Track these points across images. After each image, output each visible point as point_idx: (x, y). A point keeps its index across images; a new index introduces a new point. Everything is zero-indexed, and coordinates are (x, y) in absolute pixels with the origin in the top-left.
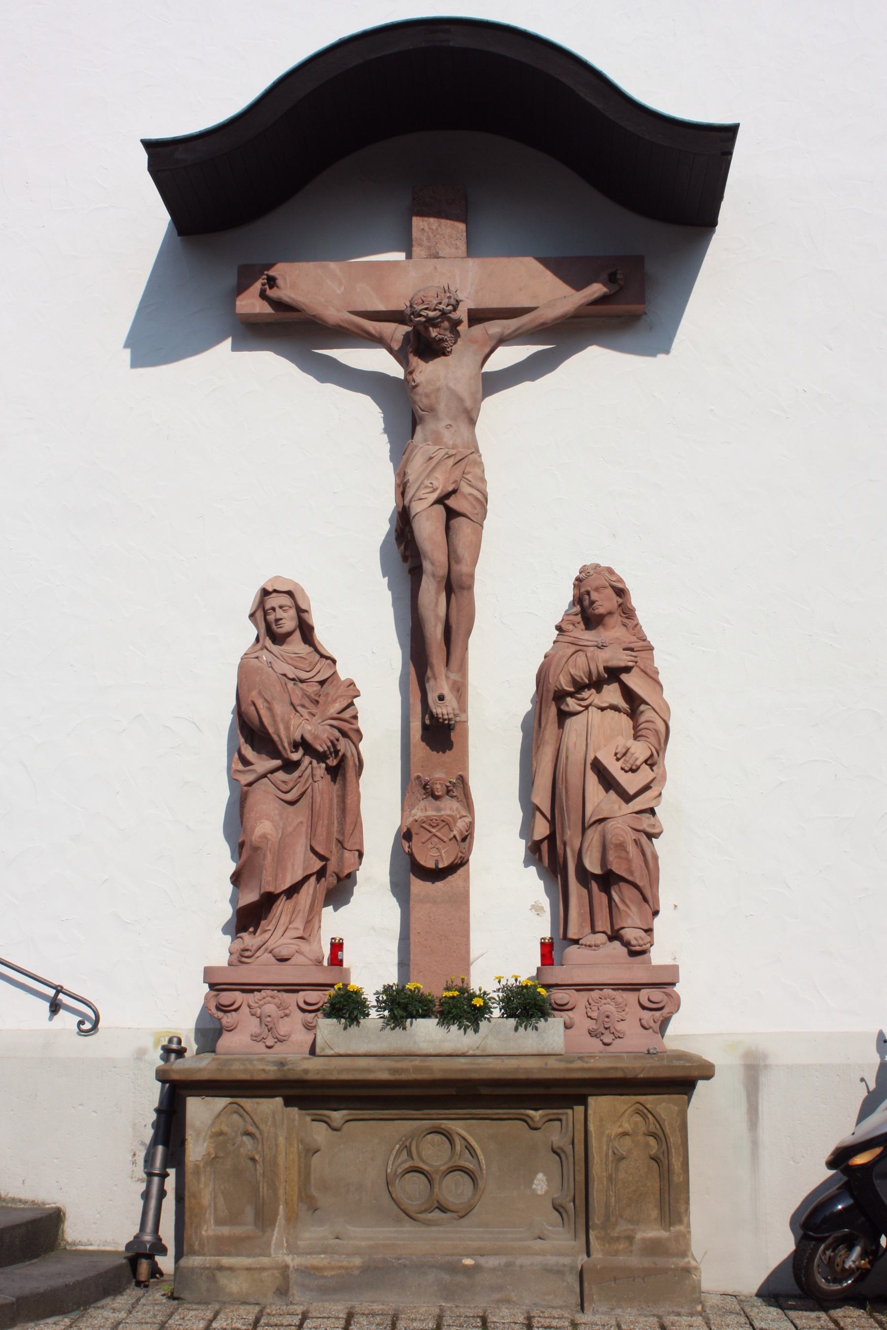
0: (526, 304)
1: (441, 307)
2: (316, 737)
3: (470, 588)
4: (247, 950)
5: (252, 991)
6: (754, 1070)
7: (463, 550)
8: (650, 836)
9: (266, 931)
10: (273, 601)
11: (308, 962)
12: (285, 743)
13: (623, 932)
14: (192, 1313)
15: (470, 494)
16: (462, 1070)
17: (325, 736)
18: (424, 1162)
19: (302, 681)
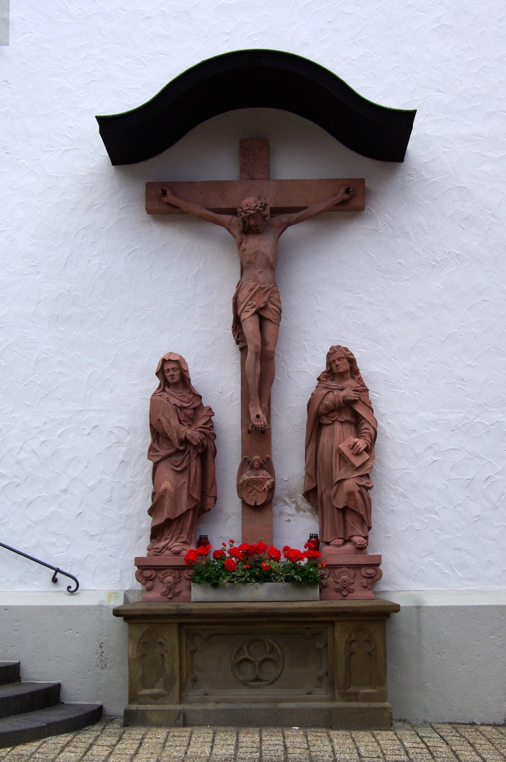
0: (302, 205)
2: (193, 437)
8: (367, 488)
15: (273, 309)
18: (251, 656)
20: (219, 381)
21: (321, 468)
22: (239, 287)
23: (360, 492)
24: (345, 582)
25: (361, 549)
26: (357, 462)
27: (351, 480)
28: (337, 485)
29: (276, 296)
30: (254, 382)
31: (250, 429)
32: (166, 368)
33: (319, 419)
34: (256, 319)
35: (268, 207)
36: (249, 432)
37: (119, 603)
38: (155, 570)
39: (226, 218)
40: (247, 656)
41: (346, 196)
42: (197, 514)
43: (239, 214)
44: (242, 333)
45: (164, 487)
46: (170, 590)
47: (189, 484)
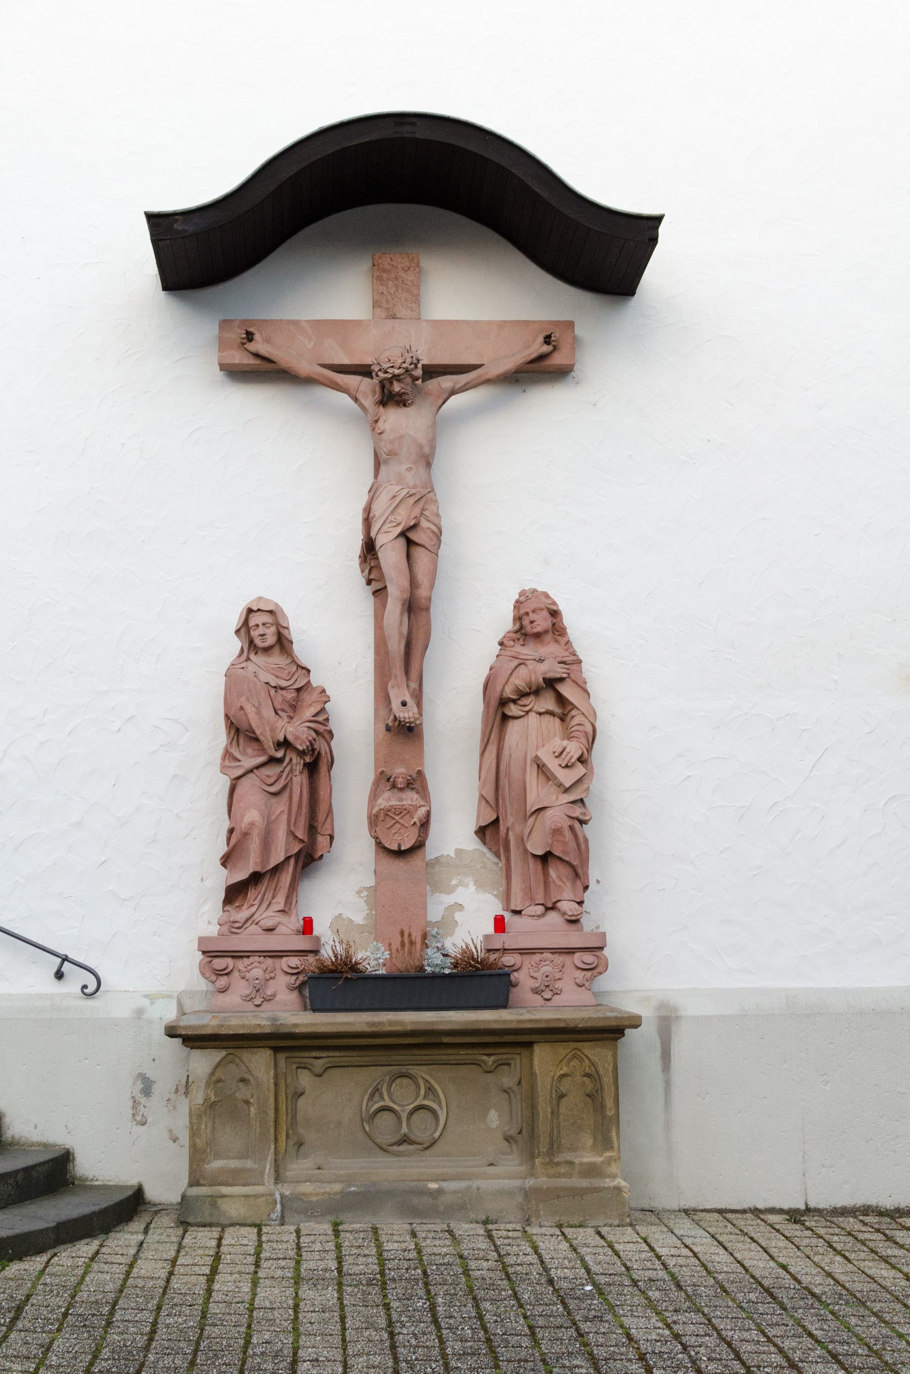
0: (473, 361)
1: (404, 365)
2: (297, 738)
3: (428, 609)
4: (236, 922)
5: (242, 957)
6: (667, 1022)
7: (422, 577)
8: (582, 822)
9: (252, 905)
10: (255, 620)
11: (290, 932)
12: (276, 745)
13: (559, 905)
14: (202, 1234)
15: (428, 528)
16: (429, 1023)
17: (304, 737)
18: (393, 1102)
19: (282, 689)
20: (338, 647)
21: (507, 790)
22: (373, 492)
23: (571, 828)
24: (547, 976)
25: (574, 922)
26: (567, 778)
27: (557, 809)
28: (534, 816)
29: (432, 507)
30: (396, 646)
31: (390, 724)
32: (252, 623)
33: (501, 710)
34: (402, 542)
35: (420, 366)
36: (388, 729)
37: (170, 1014)
38: (233, 957)
39: (352, 380)
40: (388, 1103)
41: (546, 349)
42: (300, 864)
43: (374, 374)
44: (379, 567)
45: (250, 820)
46: (258, 991)
47: (290, 814)
